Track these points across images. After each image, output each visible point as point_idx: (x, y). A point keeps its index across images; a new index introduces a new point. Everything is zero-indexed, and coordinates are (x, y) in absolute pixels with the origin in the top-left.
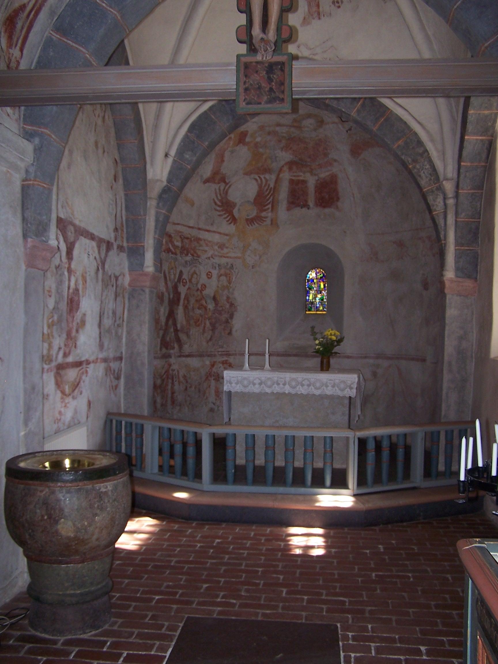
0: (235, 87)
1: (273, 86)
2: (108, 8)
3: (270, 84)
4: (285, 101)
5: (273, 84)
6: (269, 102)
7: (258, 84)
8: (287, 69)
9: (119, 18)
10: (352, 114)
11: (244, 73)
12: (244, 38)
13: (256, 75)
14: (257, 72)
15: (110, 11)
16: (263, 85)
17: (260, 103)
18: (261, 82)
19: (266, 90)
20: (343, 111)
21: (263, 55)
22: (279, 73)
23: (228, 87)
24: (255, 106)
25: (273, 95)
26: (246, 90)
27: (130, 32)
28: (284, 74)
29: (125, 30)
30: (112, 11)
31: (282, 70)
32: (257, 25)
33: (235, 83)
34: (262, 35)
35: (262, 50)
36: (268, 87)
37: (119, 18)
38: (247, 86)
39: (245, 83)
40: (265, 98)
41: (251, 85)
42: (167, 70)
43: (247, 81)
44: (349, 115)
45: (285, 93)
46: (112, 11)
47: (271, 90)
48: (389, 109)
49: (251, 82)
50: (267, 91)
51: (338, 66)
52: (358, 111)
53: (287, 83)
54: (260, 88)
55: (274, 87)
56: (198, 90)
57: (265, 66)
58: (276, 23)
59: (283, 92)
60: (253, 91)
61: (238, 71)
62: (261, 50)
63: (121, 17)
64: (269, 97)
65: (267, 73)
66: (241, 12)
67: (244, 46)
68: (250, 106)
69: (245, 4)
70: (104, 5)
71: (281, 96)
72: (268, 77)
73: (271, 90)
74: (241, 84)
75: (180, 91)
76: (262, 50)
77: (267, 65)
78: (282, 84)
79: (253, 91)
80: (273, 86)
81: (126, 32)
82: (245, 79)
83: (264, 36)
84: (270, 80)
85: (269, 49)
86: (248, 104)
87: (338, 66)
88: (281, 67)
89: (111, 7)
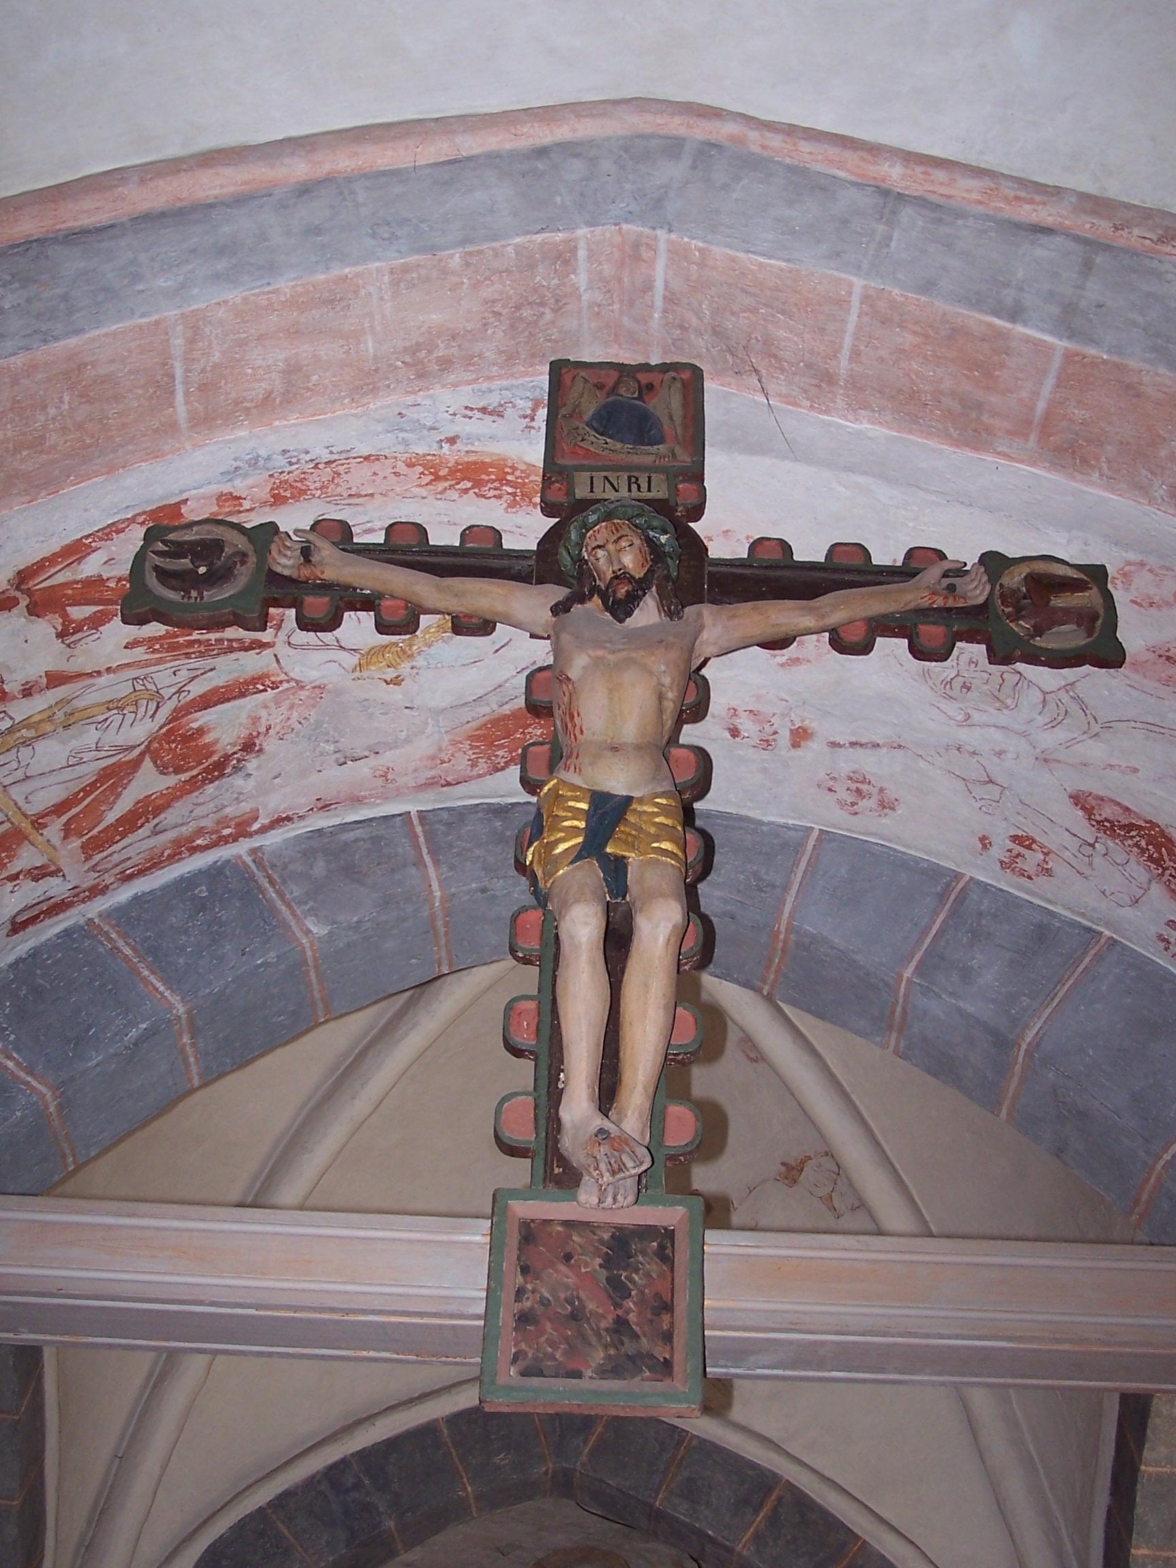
0: (480, 1309)
1: (628, 1312)
2: (22, 1074)
3: (617, 1305)
4: (676, 1369)
5: (631, 1305)
6: (612, 1370)
7: (571, 1303)
8: (682, 1256)
9: (52, 1109)
10: (739, 1548)
11: (518, 1258)
12: (523, 1132)
13: (562, 1268)
14: (568, 1257)
15: (27, 1084)
16: (591, 1306)
17: (577, 1375)
18: (583, 1295)
19: (603, 1324)
20: (709, 1536)
21: (602, 1191)
22: (654, 1267)
23: (452, 1308)
24: (560, 1384)
25: (629, 1347)
26: (524, 1319)
27: (80, 1167)
28: (672, 1271)
29: (64, 1156)
30: (34, 1083)
31: (665, 1257)
32: (584, 1086)
33: (484, 1294)
34: (599, 1121)
35: (603, 1166)
36: (610, 1318)
37: (52, 1109)
38: (528, 1304)
39: (520, 1293)
40: (598, 1356)
41: (544, 1302)
42: (226, 1226)
43: (529, 1287)
44: (730, 1550)
45: (675, 1339)
46: (34, 1083)
47: (621, 1324)
48: (858, 1537)
49: (546, 1295)
50: (607, 1330)
51: (873, 1256)
52: (758, 1538)
53: (682, 1303)
54: (576, 1316)
55: (632, 1317)
56: (333, 1310)
57: (601, 1241)
58: (651, 1090)
59: (668, 1337)
60: (548, 1326)
61: (495, 1248)
62: (597, 1168)
63: (60, 1107)
64: (612, 1352)
65: (607, 1263)
66: (517, 1052)
67: (523, 1166)
68: (535, 1382)
69: (533, 1027)
70: (10, 1064)
71: (661, 1353)
72: (608, 1279)
73: (621, 1324)
74: (507, 1296)
75: (258, 1307)
76: (603, 1166)
77: (606, 1236)
78: (667, 1307)
79: (548, 1326)
80: (628, 1312)
81: (66, 1166)
82: (520, 1279)
83: (607, 1125)
84: (617, 1289)
85: (630, 1164)
86: (524, 1373)
87: (873, 1256)
88: (662, 1247)
89: (30, 1073)
